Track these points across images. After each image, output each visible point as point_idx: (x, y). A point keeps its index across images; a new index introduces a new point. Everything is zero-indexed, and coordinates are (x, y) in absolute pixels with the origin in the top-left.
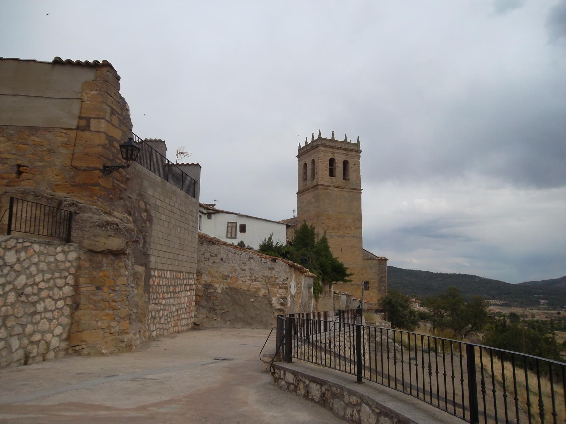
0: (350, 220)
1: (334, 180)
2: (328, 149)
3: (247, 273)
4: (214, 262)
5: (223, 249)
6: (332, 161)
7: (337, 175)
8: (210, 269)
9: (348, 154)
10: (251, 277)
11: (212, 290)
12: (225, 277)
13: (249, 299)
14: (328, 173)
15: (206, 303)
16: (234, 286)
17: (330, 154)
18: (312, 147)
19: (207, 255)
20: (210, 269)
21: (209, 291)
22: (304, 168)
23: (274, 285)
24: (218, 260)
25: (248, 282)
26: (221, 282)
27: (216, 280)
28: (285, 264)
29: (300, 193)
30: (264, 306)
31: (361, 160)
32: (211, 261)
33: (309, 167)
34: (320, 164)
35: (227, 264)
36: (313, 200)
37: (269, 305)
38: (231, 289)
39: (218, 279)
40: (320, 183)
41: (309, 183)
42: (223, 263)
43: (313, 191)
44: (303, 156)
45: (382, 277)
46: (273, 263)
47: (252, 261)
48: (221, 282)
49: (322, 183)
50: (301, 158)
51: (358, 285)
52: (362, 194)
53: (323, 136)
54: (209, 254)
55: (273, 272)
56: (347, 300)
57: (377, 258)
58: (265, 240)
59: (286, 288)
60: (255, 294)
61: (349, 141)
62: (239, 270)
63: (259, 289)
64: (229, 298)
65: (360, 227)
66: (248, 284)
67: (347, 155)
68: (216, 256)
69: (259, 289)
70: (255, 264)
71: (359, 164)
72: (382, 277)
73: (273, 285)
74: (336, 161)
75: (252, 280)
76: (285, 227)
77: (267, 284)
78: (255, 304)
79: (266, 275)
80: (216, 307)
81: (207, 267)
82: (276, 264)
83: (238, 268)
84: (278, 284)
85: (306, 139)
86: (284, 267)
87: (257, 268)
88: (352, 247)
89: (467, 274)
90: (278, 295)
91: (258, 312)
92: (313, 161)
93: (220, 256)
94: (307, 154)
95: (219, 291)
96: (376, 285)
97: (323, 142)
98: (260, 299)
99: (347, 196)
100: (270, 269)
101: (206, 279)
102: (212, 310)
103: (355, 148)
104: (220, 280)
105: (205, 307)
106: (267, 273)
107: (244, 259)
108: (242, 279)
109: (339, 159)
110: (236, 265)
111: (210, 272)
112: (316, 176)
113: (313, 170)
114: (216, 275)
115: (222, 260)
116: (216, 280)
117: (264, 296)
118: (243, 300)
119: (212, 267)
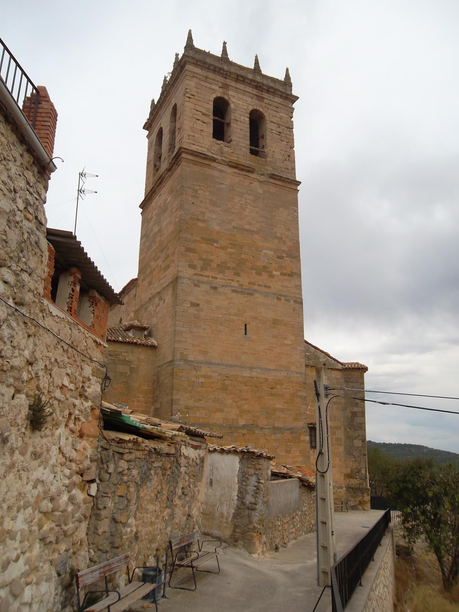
0: (271, 253)
1: (226, 149)
6: (221, 108)
9: (263, 98)
14: (210, 129)
51: (292, 430)
52: (299, 195)
56: (243, 478)
57: (340, 367)
65: (296, 274)
67: (261, 99)
74: (232, 106)
88: (275, 322)
89: (413, 444)
96: (340, 434)
109: (241, 105)
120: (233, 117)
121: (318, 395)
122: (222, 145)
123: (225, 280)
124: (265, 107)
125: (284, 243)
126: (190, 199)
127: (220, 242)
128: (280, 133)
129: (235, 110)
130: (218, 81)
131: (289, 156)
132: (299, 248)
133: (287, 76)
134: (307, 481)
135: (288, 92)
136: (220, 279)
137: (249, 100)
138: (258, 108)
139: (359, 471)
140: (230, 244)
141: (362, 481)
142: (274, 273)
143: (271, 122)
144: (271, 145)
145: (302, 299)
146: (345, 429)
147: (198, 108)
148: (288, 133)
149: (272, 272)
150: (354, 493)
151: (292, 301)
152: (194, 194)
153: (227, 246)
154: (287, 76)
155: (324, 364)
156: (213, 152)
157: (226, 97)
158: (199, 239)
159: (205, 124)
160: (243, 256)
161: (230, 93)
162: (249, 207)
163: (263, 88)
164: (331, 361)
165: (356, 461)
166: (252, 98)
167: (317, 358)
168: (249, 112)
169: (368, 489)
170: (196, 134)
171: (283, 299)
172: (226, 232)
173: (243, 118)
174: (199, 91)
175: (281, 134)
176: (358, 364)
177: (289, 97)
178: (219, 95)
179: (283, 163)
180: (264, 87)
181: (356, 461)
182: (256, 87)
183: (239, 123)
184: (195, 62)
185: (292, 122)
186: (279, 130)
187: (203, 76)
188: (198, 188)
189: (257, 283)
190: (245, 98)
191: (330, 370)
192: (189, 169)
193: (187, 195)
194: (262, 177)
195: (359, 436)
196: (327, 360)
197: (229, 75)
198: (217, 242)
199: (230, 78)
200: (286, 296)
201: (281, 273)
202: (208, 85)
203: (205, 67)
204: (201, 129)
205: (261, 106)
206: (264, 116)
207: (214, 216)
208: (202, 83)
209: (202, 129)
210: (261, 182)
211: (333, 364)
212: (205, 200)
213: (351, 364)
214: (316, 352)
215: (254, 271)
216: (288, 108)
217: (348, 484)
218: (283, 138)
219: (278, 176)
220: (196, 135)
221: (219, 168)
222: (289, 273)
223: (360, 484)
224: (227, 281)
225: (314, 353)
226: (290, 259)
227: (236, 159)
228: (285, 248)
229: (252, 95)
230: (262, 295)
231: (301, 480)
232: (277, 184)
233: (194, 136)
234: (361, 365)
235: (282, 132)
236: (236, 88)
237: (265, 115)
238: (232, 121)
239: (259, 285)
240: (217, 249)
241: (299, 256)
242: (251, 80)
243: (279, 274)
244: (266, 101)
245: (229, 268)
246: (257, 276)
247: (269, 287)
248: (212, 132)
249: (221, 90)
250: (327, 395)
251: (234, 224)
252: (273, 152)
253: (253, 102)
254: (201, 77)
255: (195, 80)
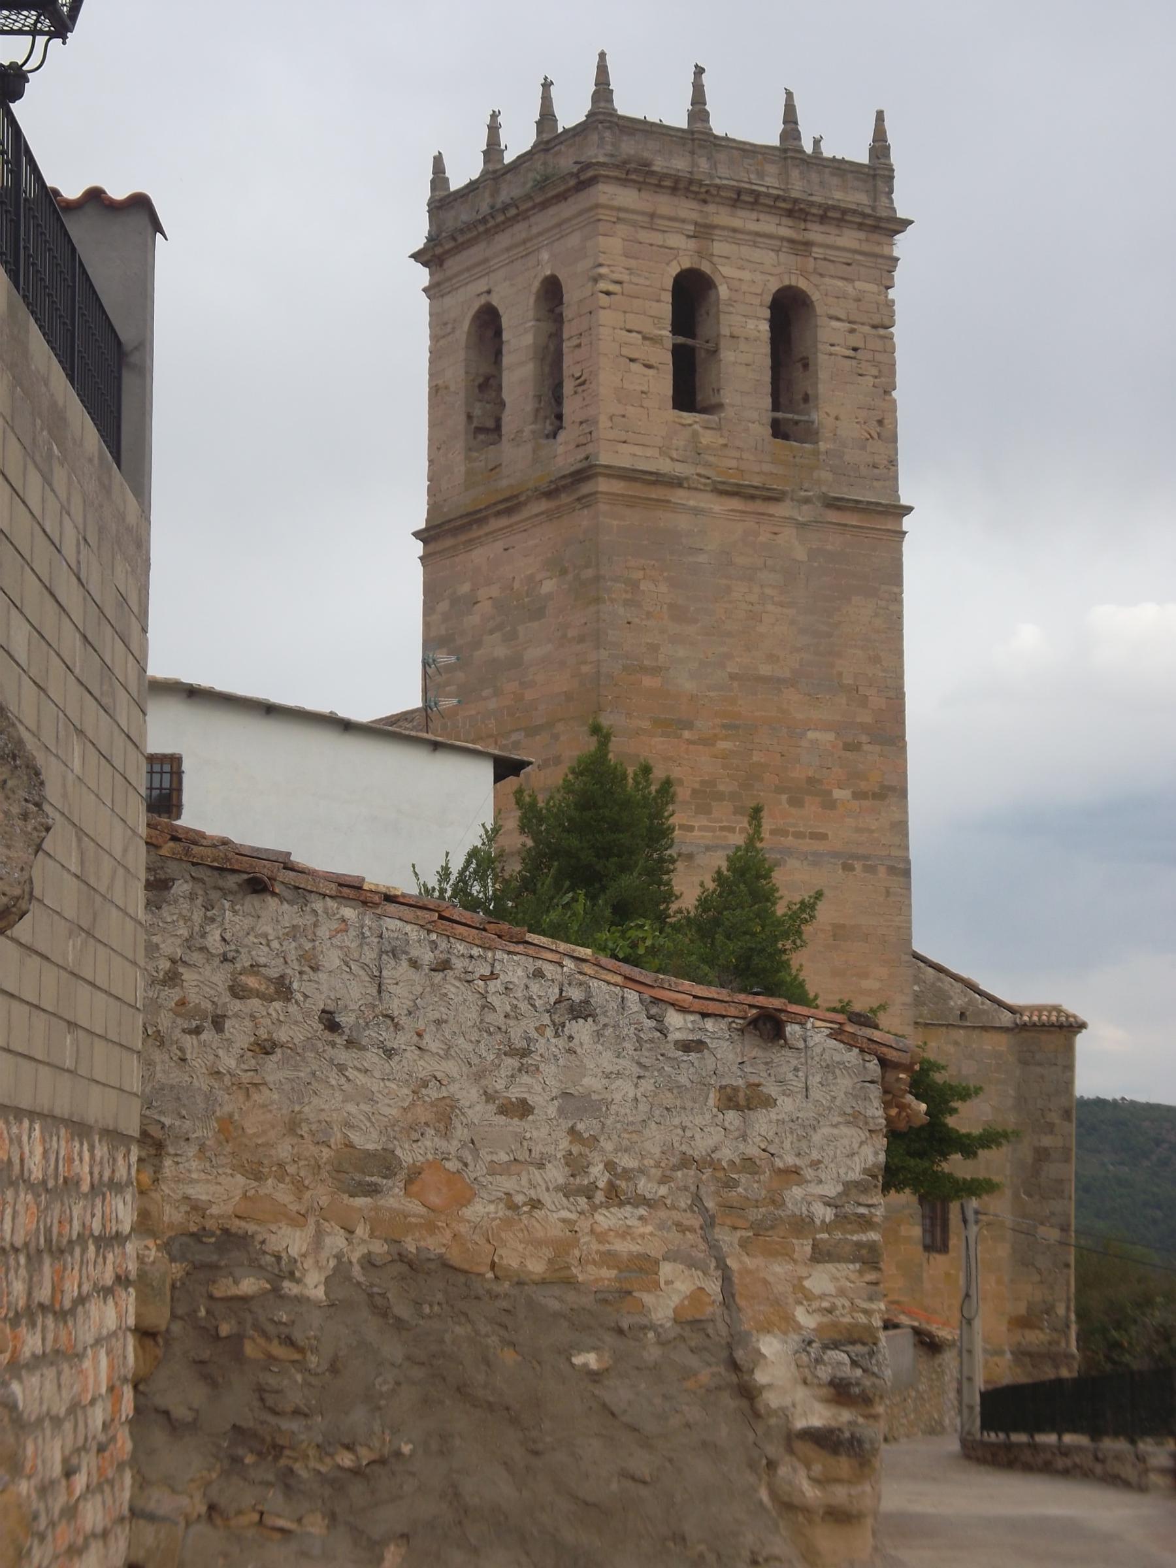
2: (665, 204)
3: (546, 1133)
4: (266, 1048)
5: (338, 933)
6: (691, 295)
8: (229, 1104)
9: (808, 244)
10: (576, 1165)
11: (249, 1285)
12: (364, 1172)
13: (565, 1354)
14: (663, 384)
15: (198, 1394)
16: (434, 1244)
17: (676, 240)
18: (542, 184)
19: (205, 983)
20: (229, 1104)
21: (224, 1288)
22: (472, 351)
23: (772, 1229)
24: (294, 1026)
25: (557, 1213)
26: (324, 1214)
27: (283, 1194)
28: (853, 1056)
29: (440, 535)
30: (694, 1413)
31: (905, 291)
32: (239, 1033)
33: (520, 336)
34: (605, 317)
35: (372, 1057)
36: (548, 586)
37: (729, 1402)
38: (412, 1267)
39: (300, 1187)
40: (605, 459)
41: (518, 459)
42: (343, 1056)
43: (550, 516)
44: (476, 252)
45: (1042, 1155)
46: (753, 1050)
47: (582, 1030)
48: (324, 1214)
49: (623, 457)
50: (453, 265)
52: (907, 545)
53: (626, 105)
54: (220, 978)
55: (762, 1123)
57: (1006, 1018)
58: (445, 873)
60: (611, 1314)
61: (808, 148)
62: (477, 1110)
63: (643, 1268)
64: (393, 1349)
65: (893, 791)
66: (557, 1231)
67: (802, 247)
68: (282, 990)
69: (643, 1268)
70: (607, 1060)
71: (883, 323)
72: (1042, 1155)
73: (759, 1229)
74: (723, 291)
75: (588, 1192)
76: (486, 771)
77: (710, 1222)
78: (619, 1394)
79: (701, 1146)
80: (287, 1425)
81: (202, 1083)
82: (784, 1060)
83: (468, 1095)
84: (802, 1225)
85: (494, 129)
86: (845, 1083)
87: (624, 1089)
90: (806, 1319)
91: (642, 1463)
92: (552, 292)
93: (319, 990)
94: (503, 240)
95: (314, 1286)
97: (629, 147)
98: (653, 1353)
99: (800, 553)
100: (730, 1100)
101: (218, 1191)
102: (254, 1446)
103: (856, 198)
104: (321, 1194)
105: (193, 1426)
106: (710, 1133)
107: (514, 1014)
108: (507, 1184)
110: (451, 1067)
111: (228, 1128)
112: (571, 408)
113: (551, 358)
114: (284, 1150)
115: (332, 1026)
116: (283, 1194)
117: (691, 1323)
118: (509, 1357)
119: (247, 1090)
120: (725, 331)
121: (965, 1221)
122: (696, 427)
123: (713, 830)
124: (815, 271)
125: (864, 702)
126: (621, 611)
127: (699, 724)
128: (855, 349)
129: (731, 302)
130: (683, 221)
131: (880, 422)
132: (904, 711)
133: (880, 147)
134: (930, 1335)
135: (884, 214)
136: (701, 829)
137: (768, 258)
138: (793, 283)
139: (1049, 1310)
140: (724, 726)
141: (1055, 1336)
142: (838, 794)
143: (831, 318)
144: (835, 405)
145: (908, 862)
146: (1016, 1196)
147: (633, 322)
148: (878, 344)
149: (830, 793)
150: (1034, 1366)
151: (882, 871)
152: (629, 596)
153: (715, 735)
154: (880, 147)
155: (962, 1015)
156: (675, 456)
157: (706, 267)
158: (646, 724)
159: (651, 372)
160: (756, 758)
161: (719, 248)
162: (770, 607)
163: (807, 214)
164: (983, 1003)
165: (1041, 1282)
166: (777, 251)
167: (942, 996)
168: (768, 299)
169: (1073, 1356)
170: (630, 408)
171: (858, 866)
172: (712, 694)
173: (751, 324)
174: (633, 263)
175: (859, 355)
176: (1057, 1009)
177: (883, 225)
178: (687, 264)
179: (864, 448)
180: (814, 211)
181: (1041, 1282)
182: (790, 213)
183: (743, 346)
184: (624, 176)
185: (890, 304)
186: (854, 341)
187: (643, 213)
188: (640, 574)
189: (791, 830)
190: (757, 255)
191: (977, 1032)
192: (615, 523)
193: (612, 600)
194: (805, 507)
195: (1053, 1214)
196: (971, 1002)
197: (715, 192)
198: (689, 725)
199: (718, 199)
200: (866, 857)
201: (854, 793)
202: (657, 238)
203: (649, 184)
204: (639, 388)
205: (803, 273)
206: (812, 302)
207: (681, 652)
208: (644, 236)
209: (645, 389)
210: (801, 526)
211: (984, 1012)
212: (658, 608)
213: (1040, 1009)
214: (939, 979)
215: (784, 797)
216: (880, 261)
217: (1019, 1344)
218: (864, 364)
219: (848, 500)
220: (631, 411)
221: (692, 503)
222: (877, 790)
223: (1050, 1343)
224: (718, 833)
225: (933, 984)
226: (878, 748)
227: (733, 464)
228: (866, 718)
229: (778, 243)
230: (805, 863)
231: (917, 1332)
232: (845, 525)
233: (624, 416)
234: (1068, 1016)
235: (861, 345)
236: (735, 230)
237: (814, 298)
238: (723, 343)
239: (799, 835)
240: (691, 747)
241: (902, 737)
242: (777, 198)
243: (849, 797)
244: (817, 251)
245: (720, 797)
246: (793, 810)
247: (823, 837)
248: (670, 393)
249: (692, 244)
250: (977, 1222)
251: (732, 668)
252: (837, 418)
253: (779, 264)
254: (640, 218)
255: (622, 230)
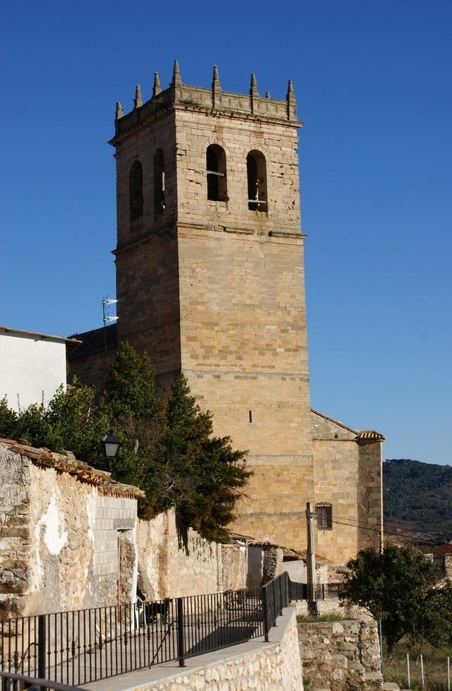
1: (223, 210)
7: (230, 194)
14: (204, 190)
29: (122, 252)
59: (24, 535)
72: (369, 490)
88: (281, 405)
96: (354, 513)
99: (261, 255)
149: (275, 350)
171: (288, 378)
247: (274, 367)
251: (234, 301)
